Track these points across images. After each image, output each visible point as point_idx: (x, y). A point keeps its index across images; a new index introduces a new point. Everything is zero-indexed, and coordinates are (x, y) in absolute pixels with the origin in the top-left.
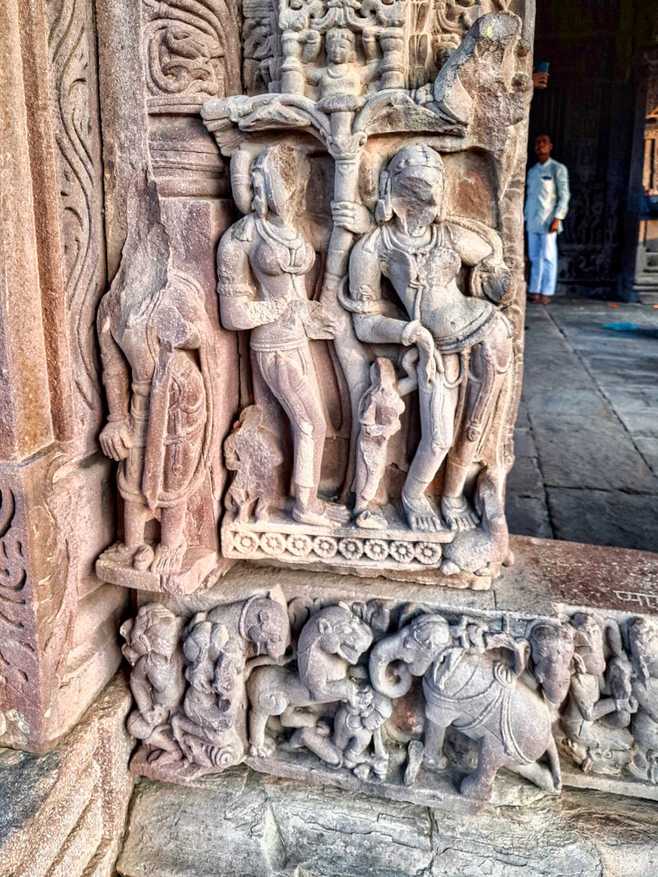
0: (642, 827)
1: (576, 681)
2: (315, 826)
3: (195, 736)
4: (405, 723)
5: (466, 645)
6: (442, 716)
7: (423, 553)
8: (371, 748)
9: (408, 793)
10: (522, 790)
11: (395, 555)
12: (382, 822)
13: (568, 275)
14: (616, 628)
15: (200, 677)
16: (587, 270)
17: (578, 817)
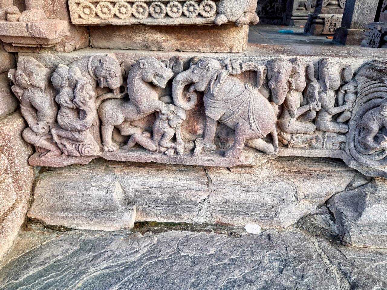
0: (316, 173)
1: (289, 95)
2: (144, 187)
3: (68, 139)
4: (193, 130)
5: (230, 68)
6: (215, 112)
7: (204, 10)
8: (174, 139)
9: (196, 160)
10: (256, 156)
11: (187, 13)
12: (181, 181)
13: (261, 13)
14: (312, 65)
15: (64, 98)
16: (270, 11)
17: (284, 172)
